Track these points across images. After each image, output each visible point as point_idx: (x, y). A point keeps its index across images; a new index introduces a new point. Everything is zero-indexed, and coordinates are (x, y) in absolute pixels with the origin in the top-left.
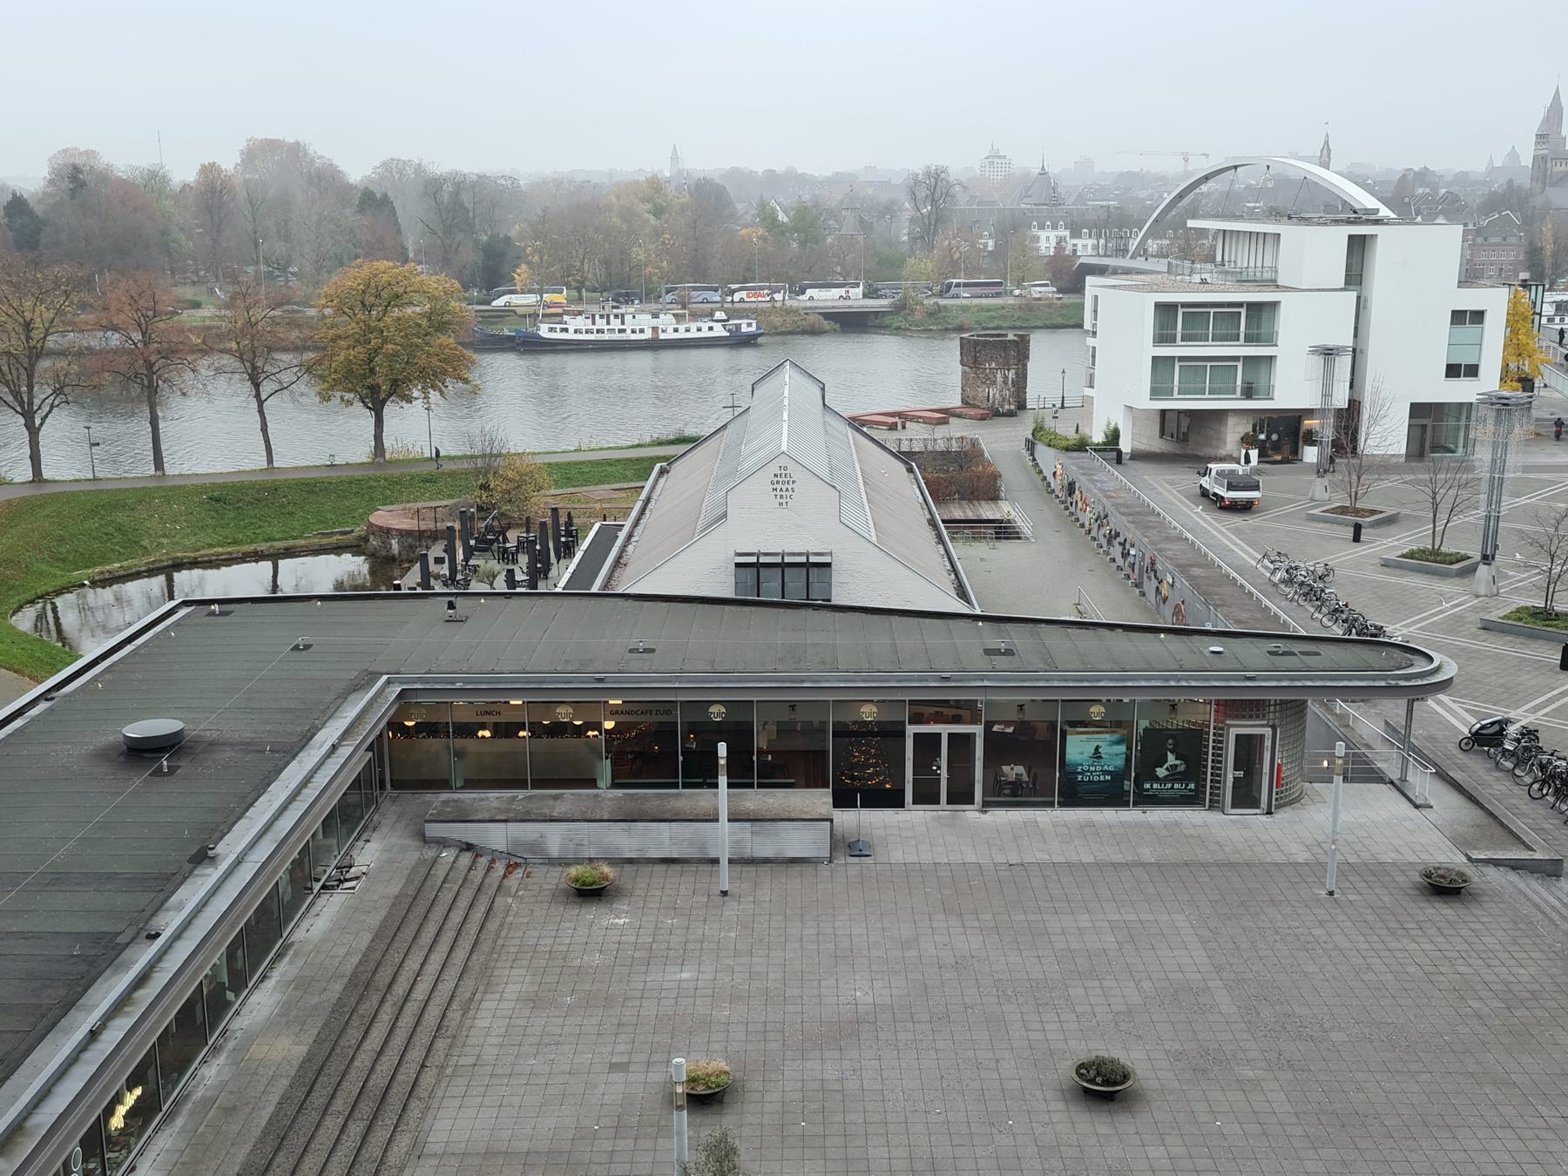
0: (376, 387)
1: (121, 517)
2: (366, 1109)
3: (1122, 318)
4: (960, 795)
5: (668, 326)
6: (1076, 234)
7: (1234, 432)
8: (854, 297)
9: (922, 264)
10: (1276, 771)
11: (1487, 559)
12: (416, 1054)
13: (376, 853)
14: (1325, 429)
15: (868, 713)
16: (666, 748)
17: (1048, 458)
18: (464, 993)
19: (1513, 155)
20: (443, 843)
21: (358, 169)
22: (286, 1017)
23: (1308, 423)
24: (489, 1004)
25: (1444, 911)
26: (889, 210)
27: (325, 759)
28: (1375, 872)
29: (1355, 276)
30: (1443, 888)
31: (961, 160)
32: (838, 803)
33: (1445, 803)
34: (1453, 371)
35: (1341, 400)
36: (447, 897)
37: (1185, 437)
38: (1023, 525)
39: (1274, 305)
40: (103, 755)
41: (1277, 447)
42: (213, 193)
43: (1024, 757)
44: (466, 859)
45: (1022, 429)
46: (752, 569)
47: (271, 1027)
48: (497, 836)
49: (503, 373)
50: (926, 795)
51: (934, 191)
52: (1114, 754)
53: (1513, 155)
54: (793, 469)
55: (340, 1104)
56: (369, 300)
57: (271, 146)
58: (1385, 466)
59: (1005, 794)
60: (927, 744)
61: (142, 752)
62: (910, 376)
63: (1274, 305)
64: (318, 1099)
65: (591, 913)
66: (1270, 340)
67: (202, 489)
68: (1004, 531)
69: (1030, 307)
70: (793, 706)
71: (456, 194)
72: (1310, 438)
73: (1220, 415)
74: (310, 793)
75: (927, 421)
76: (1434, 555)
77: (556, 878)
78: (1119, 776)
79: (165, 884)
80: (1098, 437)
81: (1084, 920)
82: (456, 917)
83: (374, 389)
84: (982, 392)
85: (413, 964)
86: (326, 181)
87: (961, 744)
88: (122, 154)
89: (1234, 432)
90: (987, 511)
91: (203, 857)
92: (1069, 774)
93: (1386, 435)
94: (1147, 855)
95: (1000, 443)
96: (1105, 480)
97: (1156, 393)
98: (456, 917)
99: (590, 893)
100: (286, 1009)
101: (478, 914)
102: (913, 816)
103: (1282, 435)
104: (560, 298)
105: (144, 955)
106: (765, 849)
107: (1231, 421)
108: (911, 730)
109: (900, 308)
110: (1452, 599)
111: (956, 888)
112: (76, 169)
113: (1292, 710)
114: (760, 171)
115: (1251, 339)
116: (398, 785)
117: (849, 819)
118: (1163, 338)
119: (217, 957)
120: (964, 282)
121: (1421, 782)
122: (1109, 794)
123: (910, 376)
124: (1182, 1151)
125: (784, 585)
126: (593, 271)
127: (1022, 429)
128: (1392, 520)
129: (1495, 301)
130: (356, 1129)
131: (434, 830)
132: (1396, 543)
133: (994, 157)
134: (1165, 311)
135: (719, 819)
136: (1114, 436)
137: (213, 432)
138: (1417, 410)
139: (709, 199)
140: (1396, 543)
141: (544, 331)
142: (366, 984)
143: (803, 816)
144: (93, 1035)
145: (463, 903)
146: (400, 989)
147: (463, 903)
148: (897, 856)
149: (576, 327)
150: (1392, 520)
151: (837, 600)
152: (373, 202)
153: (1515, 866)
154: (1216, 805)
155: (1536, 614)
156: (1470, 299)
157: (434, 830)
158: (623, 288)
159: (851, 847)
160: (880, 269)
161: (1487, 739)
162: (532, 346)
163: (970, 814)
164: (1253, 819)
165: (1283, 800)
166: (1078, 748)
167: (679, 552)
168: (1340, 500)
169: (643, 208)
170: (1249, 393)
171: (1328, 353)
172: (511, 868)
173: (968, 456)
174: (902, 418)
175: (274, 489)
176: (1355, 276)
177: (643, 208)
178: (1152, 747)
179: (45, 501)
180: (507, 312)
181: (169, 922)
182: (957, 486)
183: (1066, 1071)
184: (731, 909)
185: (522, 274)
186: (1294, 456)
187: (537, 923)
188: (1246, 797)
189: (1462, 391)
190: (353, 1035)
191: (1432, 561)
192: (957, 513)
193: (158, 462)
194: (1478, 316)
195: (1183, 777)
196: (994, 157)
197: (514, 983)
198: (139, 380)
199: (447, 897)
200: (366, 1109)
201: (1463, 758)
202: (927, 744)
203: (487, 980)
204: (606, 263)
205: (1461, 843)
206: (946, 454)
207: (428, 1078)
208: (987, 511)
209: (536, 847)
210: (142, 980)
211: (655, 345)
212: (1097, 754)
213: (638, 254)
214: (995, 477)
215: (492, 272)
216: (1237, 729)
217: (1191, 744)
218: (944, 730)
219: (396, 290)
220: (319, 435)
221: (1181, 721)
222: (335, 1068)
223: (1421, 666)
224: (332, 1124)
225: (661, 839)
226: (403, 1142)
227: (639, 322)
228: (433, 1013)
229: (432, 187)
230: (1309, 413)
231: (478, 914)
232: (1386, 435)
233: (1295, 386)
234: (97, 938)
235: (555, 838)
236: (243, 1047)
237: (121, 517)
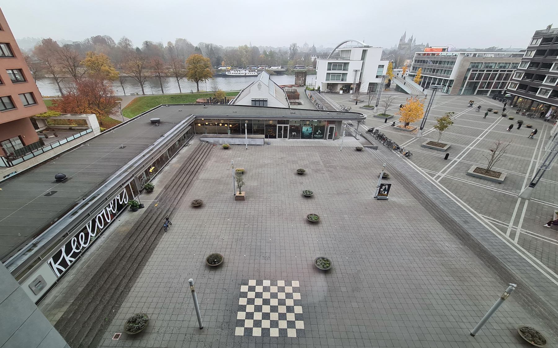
0: (197, 76)
1: (157, 100)
2: (190, 173)
3: (322, 67)
4: (285, 137)
5: (247, 73)
6: (318, 58)
7: (339, 87)
8: (279, 68)
9: (291, 62)
10: (335, 134)
11: (376, 106)
12: (198, 167)
13: (194, 142)
14: (354, 87)
15: (271, 122)
16: (238, 128)
17: (308, 92)
18: (206, 160)
19: (396, 45)
20: (203, 141)
21: (195, 45)
22: (178, 162)
23: (352, 86)
24: (209, 162)
25: (358, 153)
26: (286, 53)
27: (182, 125)
28: (349, 148)
29: (363, 58)
30: (359, 150)
31: (301, 46)
32: (266, 137)
33: (362, 140)
34: (377, 77)
35: (357, 82)
36: (204, 148)
37: (331, 87)
38: (303, 103)
39: (349, 63)
40: (148, 123)
41: (346, 90)
42: (170, 49)
43: (296, 132)
44: (207, 144)
45: (305, 88)
46: (254, 101)
47: (176, 163)
48: (211, 140)
49: (220, 80)
50: (280, 137)
51: (294, 52)
52: (310, 130)
53: (396, 45)
54: (261, 83)
55: (186, 173)
56: (195, 61)
57: (181, 39)
58: (363, 94)
59: (292, 137)
60: (280, 128)
61: (153, 123)
62: (288, 80)
63: (349, 63)
64: (183, 171)
65: (226, 151)
66: (347, 70)
67: (170, 96)
68: (299, 104)
69: (309, 70)
70: (259, 121)
71: (211, 48)
72: (352, 89)
73: (338, 84)
74: (180, 129)
75: (289, 87)
76: (368, 106)
77: (221, 146)
78: (311, 134)
79: (156, 139)
80: (316, 88)
81: (302, 153)
82: (205, 151)
83: (196, 78)
84: (298, 82)
85: (198, 156)
86: (190, 46)
87: (286, 128)
88: (155, 40)
89: (339, 87)
90: (297, 101)
91: (162, 136)
92: (303, 133)
93: (364, 88)
94: (313, 145)
95: (300, 90)
96: (316, 95)
97: (327, 80)
98: (205, 151)
99: (226, 148)
100: (178, 161)
101: (208, 151)
102: (278, 140)
103: (347, 88)
104: (230, 68)
105: (151, 147)
106: (253, 143)
107: (339, 85)
108: (278, 125)
109: (287, 70)
110: (371, 112)
111: (283, 149)
112: (147, 42)
113: (340, 123)
114: (165, 45)
115: (344, 70)
116: (197, 133)
117: (266, 140)
118: (329, 69)
119: (166, 150)
120: (297, 65)
121: (358, 137)
122: (309, 137)
123: (288, 80)
124: (326, 215)
125: (259, 103)
126: (235, 63)
127: (305, 88)
128: (363, 102)
129: (386, 63)
130: (188, 176)
131: (202, 139)
132: (362, 105)
133: (306, 44)
134: (330, 64)
135: (246, 139)
136: (319, 88)
137: (172, 88)
138: (370, 84)
139: (255, 51)
140: (362, 105)
141: (227, 73)
142: (190, 159)
143: (260, 139)
144: (144, 156)
145: (206, 149)
146: (196, 159)
147: (206, 149)
148: (274, 145)
149: (232, 73)
150: (363, 102)
151: (268, 106)
152: (198, 49)
153: (371, 148)
154: (325, 139)
155: (382, 114)
156: (382, 63)
157: (202, 139)
158: (240, 66)
159: (268, 144)
160: (284, 63)
161: (370, 131)
162: (225, 76)
163: (287, 139)
164: (331, 141)
165: (336, 138)
166: (304, 129)
167: (245, 100)
168: (355, 98)
169: (244, 51)
170: (342, 80)
171: (356, 71)
172: (214, 145)
173: (295, 92)
174: (285, 86)
175: (181, 96)
176: (363, 58)
177: (244, 51)
178: (316, 129)
179: (145, 97)
180: (221, 70)
181: (156, 143)
182: (292, 96)
183: (296, 171)
184: (248, 151)
185: (223, 63)
186: (349, 92)
187: (217, 152)
188: (330, 137)
189: (378, 81)
190: (188, 164)
191: (368, 107)
192: (292, 101)
193: (163, 92)
194: (383, 66)
195: (321, 134)
196: (306, 44)
197: (213, 159)
198: (159, 80)
199: (204, 148)
200: (190, 173)
201: (367, 134)
202: (280, 128)
203: (209, 159)
204: (237, 61)
205: (362, 144)
206: (291, 92)
207: (199, 170)
208: (297, 101)
209: (218, 142)
210: (152, 150)
211: (245, 76)
212: (307, 130)
213: (243, 59)
214: (299, 95)
215: (218, 64)
216: (330, 126)
217: (322, 129)
218: (283, 125)
219: (202, 64)
220: (187, 87)
221: (322, 124)
222: (185, 168)
223: (361, 116)
224: (184, 175)
225: (237, 141)
226: (195, 178)
227: (243, 72)
228: (200, 163)
229: (207, 46)
230: (351, 84)
231: (208, 151)
232: (364, 88)
233: (350, 79)
234: (145, 145)
235: (221, 140)
236: (172, 165)
237: (157, 100)
